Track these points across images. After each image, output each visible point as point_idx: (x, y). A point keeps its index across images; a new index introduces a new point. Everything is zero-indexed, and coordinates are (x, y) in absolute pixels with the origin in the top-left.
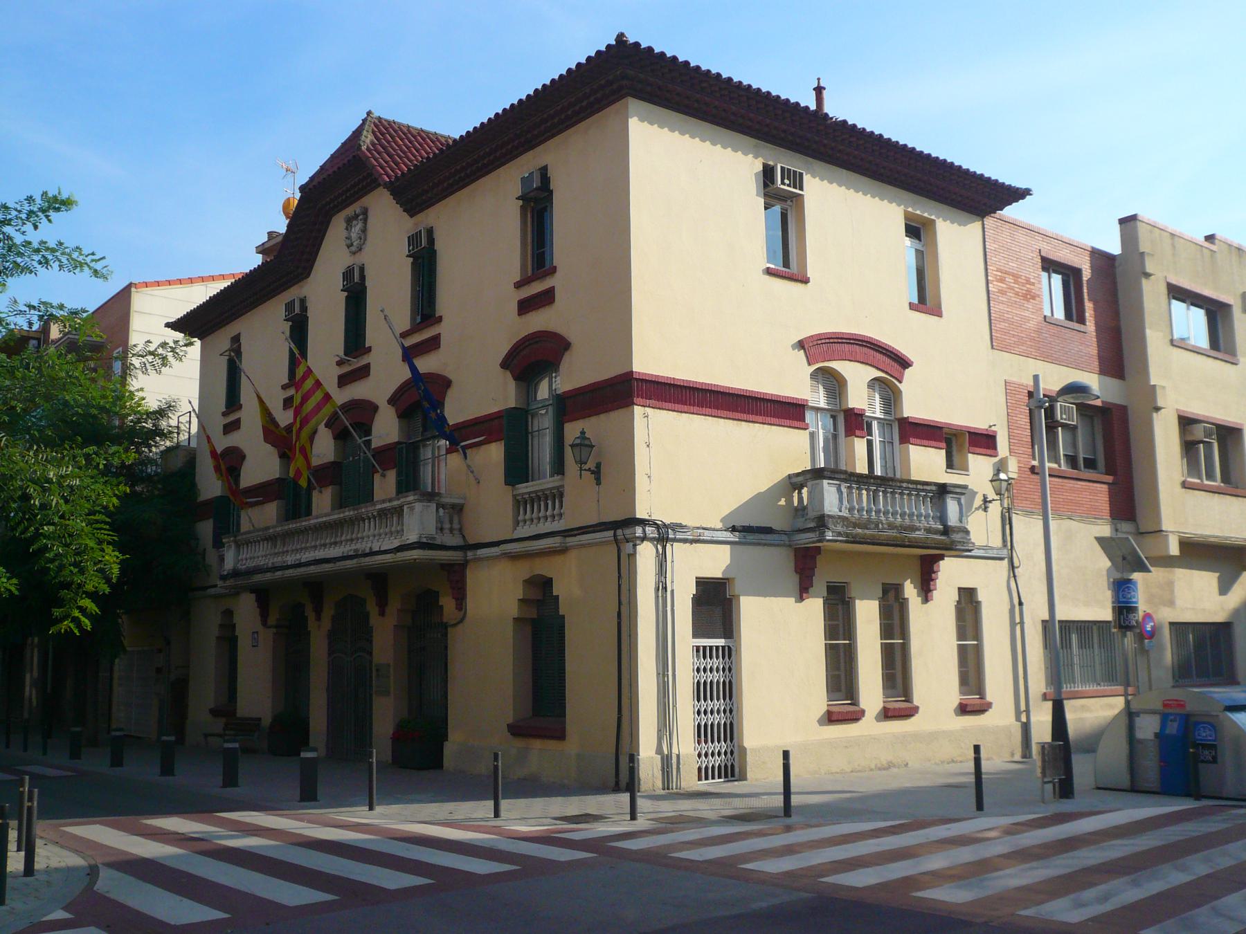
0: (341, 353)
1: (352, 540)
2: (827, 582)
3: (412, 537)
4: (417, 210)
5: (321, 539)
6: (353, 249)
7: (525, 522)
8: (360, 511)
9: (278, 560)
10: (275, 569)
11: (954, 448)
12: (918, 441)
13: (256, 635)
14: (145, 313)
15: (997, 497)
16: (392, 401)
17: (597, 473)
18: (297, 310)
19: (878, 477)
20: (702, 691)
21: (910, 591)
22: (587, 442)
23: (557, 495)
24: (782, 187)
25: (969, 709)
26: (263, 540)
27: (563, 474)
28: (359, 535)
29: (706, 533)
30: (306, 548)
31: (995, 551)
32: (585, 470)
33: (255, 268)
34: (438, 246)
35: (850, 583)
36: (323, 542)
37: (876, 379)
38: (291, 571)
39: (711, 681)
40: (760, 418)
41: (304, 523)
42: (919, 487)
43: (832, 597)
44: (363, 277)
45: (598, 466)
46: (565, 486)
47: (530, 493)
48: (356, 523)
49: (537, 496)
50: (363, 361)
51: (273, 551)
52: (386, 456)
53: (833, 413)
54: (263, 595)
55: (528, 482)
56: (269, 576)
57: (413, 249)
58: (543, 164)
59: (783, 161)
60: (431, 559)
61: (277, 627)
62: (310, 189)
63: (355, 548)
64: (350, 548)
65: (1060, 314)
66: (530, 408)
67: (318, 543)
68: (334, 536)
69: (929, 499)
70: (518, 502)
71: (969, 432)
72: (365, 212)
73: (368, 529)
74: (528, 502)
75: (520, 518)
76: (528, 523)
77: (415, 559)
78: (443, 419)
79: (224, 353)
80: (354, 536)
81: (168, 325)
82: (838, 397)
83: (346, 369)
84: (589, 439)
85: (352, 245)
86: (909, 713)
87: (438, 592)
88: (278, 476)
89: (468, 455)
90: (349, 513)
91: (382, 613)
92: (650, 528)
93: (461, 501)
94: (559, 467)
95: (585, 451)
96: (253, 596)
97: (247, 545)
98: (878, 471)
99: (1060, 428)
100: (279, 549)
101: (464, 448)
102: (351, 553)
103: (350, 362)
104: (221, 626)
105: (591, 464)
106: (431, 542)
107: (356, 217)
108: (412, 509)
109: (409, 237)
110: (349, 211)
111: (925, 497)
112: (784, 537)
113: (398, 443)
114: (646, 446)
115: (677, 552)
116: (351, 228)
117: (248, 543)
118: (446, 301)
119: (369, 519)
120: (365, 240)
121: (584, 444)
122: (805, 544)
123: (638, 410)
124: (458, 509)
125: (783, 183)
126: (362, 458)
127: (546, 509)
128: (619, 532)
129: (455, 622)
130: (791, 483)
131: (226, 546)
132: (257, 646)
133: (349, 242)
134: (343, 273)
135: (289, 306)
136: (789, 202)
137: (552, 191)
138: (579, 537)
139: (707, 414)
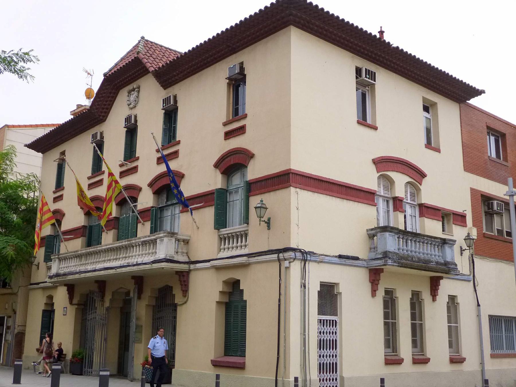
0: (122, 160)
1: (126, 257)
2: (385, 288)
3: (161, 255)
4: (168, 86)
5: (108, 257)
6: (131, 106)
7: (237, 248)
8: (131, 242)
9: (83, 268)
10: (81, 272)
11: (445, 222)
12: (429, 216)
13: (66, 309)
14: (12, 141)
15: (468, 248)
16: (151, 185)
17: (268, 223)
18: (99, 138)
19: (409, 232)
20: (321, 345)
21: (426, 296)
22: (263, 206)
23: (244, 235)
24: (366, 79)
25: (454, 361)
26: (74, 257)
27: (248, 224)
28: (130, 255)
29: (326, 258)
30: (99, 262)
31: (466, 277)
32: (262, 221)
33: (69, 120)
34: (179, 105)
35: (396, 289)
36: (109, 258)
37: (408, 183)
38: (90, 274)
39: (327, 339)
40: (353, 199)
41: (98, 248)
42: (432, 239)
43: (387, 296)
44: (136, 121)
45: (269, 219)
46: (249, 230)
47: (228, 234)
48: (129, 248)
49: (228, 236)
50: (134, 165)
51: (79, 263)
52: (145, 213)
53: (388, 199)
54: (71, 288)
55: (226, 228)
56: (77, 276)
57: (127, 124)
58: (241, 61)
59: (365, 65)
60: (172, 268)
61: (78, 304)
62: (109, 75)
63: (128, 261)
64: (125, 262)
65: (494, 155)
66: (229, 189)
67: (106, 259)
68: (115, 255)
69: (436, 246)
70: (221, 239)
71: (453, 214)
72: (139, 88)
73: (137, 251)
74: (226, 239)
75: (222, 247)
76: (226, 250)
77: (163, 268)
78: (181, 193)
79: (56, 160)
80: (127, 255)
81: (26, 146)
82: (390, 191)
83: (124, 168)
84: (265, 204)
85: (130, 104)
86: (426, 361)
87: (172, 287)
88: (83, 224)
89: (193, 213)
90: (124, 243)
91: (139, 298)
92: (298, 253)
93: (188, 238)
94: (246, 220)
95: (263, 210)
96: (65, 288)
97: (65, 260)
98: (409, 229)
99: (495, 215)
100: (83, 261)
101: (192, 210)
102: (126, 264)
103: (127, 165)
104: (46, 304)
105: (265, 219)
106: (172, 259)
107: (133, 90)
108: (162, 241)
109: (163, 100)
110: (130, 87)
111: (434, 245)
112: (365, 263)
113: (152, 207)
114: (296, 209)
115: (311, 267)
116: (130, 96)
117: (65, 259)
118: (180, 134)
119: (136, 246)
120: (138, 102)
121: (262, 207)
122: (375, 267)
123: (292, 189)
124: (186, 242)
125: (366, 77)
126: (131, 215)
127: (237, 243)
128: (281, 255)
129: (181, 303)
130: (368, 234)
131: (53, 260)
132: (66, 315)
133: (129, 102)
134: (125, 119)
135: (94, 136)
136: (367, 88)
137: (246, 75)
138: (256, 258)
139: (327, 194)
